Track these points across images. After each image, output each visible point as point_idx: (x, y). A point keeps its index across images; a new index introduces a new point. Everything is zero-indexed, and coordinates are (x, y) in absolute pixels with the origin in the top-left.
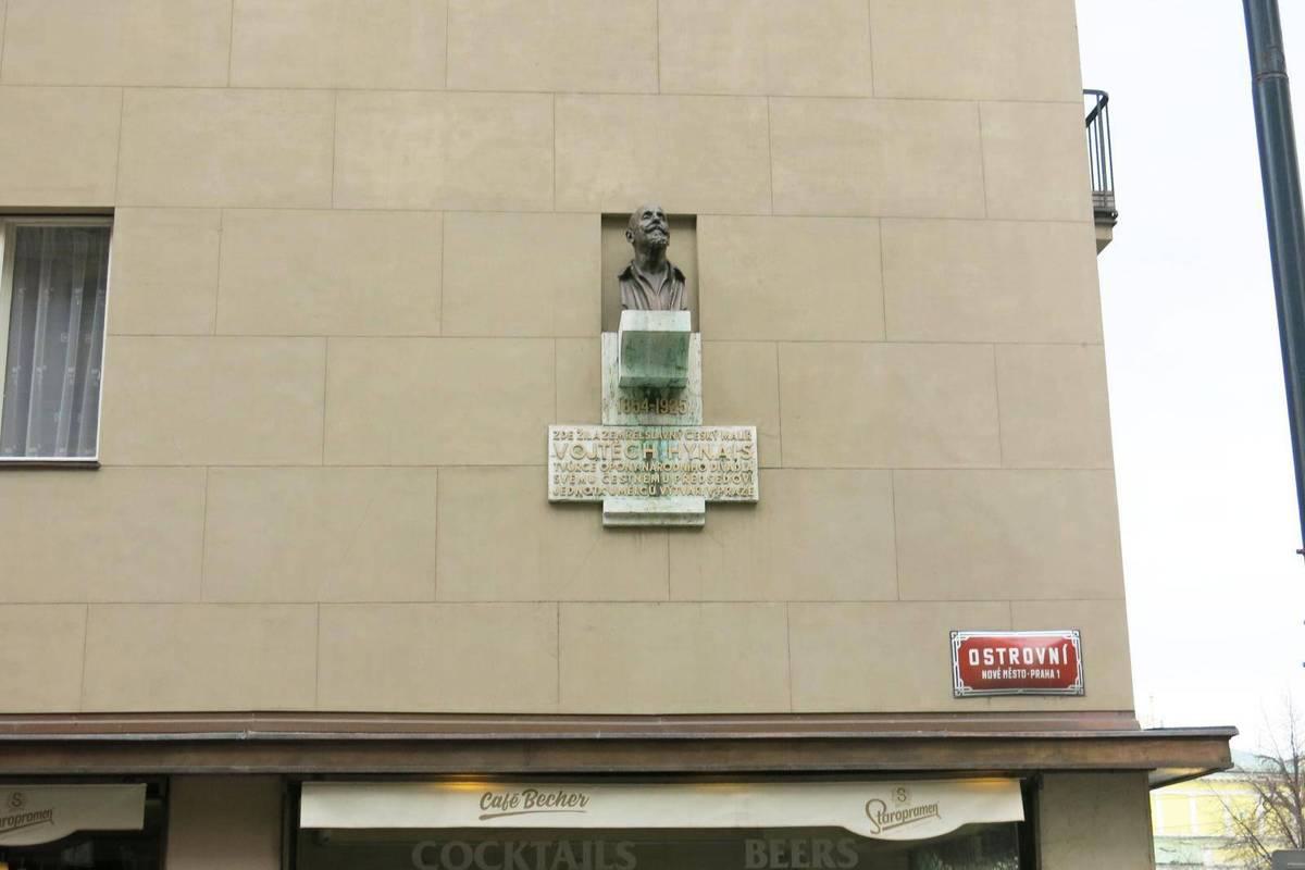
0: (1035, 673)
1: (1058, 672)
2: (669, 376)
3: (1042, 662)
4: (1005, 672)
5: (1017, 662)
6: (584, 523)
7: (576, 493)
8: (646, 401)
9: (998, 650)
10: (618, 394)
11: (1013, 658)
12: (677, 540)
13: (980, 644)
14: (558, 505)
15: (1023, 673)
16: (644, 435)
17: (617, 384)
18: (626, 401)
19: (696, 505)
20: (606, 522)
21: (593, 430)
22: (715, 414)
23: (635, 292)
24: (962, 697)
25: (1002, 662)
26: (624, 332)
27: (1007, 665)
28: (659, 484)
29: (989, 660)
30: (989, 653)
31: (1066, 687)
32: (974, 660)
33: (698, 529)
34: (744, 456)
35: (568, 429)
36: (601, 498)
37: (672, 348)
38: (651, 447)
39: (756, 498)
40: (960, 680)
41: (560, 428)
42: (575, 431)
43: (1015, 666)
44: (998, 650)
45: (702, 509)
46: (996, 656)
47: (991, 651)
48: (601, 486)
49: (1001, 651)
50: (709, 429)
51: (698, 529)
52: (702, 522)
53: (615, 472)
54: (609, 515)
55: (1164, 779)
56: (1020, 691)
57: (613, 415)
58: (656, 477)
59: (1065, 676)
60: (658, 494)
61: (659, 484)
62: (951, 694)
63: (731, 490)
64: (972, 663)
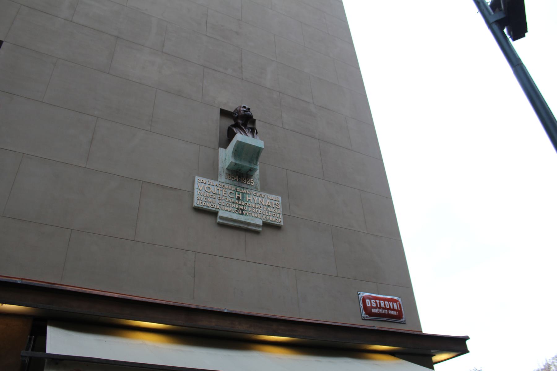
0: (390, 312)
1: (397, 312)
2: (251, 166)
3: (392, 307)
4: (380, 310)
5: (384, 307)
6: (208, 220)
7: (207, 205)
8: (237, 177)
9: (376, 301)
10: (226, 171)
11: (382, 305)
12: (249, 235)
13: (371, 298)
14: (199, 210)
15: (385, 311)
16: (236, 189)
17: (225, 168)
18: (229, 175)
19: (260, 223)
20: (219, 220)
21: (215, 183)
22: (265, 188)
23: (241, 131)
24: (365, 319)
25: (379, 306)
26: (238, 141)
27: (380, 308)
28: (243, 210)
29: (374, 304)
30: (373, 302)
31: (400, 319)
32: (368, 304)
33: (257, 233)
34: (277, 207)
35: (205, 180)
36: (218, 210)
37: (255, 153)
38: (239, 195)
39: (282, 224)
40: (364, 312)
41: (200, 178)
42: (207, 181)
43: (383, 308)
44: (376, 301)
45: (261, 224)
46: (376, 303)
47: (374, 301)
48: (218, 207)
49: (378, 301)
50: (263, 194)
51: (257, 233)
52: (261, 229)
53: (224, 201)
54: (221, 218)
55: (438, 361)
56: (385, 319)
57: (223, 178)
58: (241, 207)
59: (398, 317)
60: (242, 214)
61: (243, 210)
62: (361, 319)
63: (272, 219)
64: (368, 305)
